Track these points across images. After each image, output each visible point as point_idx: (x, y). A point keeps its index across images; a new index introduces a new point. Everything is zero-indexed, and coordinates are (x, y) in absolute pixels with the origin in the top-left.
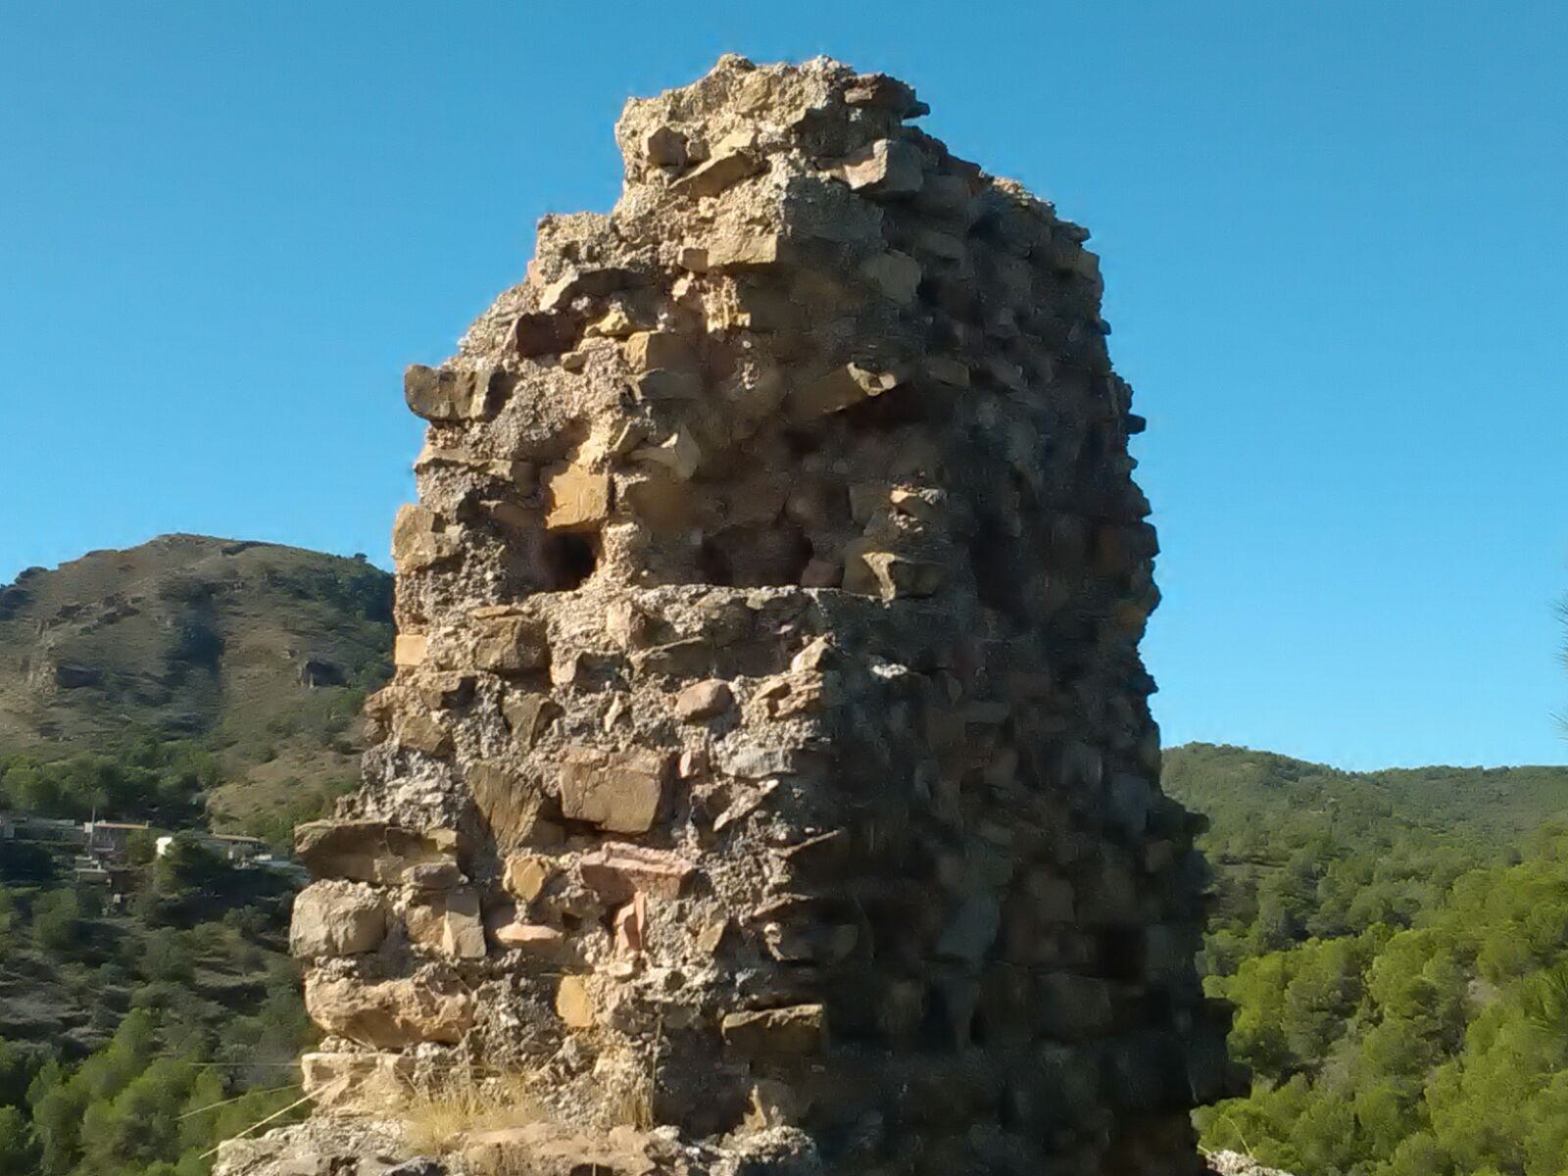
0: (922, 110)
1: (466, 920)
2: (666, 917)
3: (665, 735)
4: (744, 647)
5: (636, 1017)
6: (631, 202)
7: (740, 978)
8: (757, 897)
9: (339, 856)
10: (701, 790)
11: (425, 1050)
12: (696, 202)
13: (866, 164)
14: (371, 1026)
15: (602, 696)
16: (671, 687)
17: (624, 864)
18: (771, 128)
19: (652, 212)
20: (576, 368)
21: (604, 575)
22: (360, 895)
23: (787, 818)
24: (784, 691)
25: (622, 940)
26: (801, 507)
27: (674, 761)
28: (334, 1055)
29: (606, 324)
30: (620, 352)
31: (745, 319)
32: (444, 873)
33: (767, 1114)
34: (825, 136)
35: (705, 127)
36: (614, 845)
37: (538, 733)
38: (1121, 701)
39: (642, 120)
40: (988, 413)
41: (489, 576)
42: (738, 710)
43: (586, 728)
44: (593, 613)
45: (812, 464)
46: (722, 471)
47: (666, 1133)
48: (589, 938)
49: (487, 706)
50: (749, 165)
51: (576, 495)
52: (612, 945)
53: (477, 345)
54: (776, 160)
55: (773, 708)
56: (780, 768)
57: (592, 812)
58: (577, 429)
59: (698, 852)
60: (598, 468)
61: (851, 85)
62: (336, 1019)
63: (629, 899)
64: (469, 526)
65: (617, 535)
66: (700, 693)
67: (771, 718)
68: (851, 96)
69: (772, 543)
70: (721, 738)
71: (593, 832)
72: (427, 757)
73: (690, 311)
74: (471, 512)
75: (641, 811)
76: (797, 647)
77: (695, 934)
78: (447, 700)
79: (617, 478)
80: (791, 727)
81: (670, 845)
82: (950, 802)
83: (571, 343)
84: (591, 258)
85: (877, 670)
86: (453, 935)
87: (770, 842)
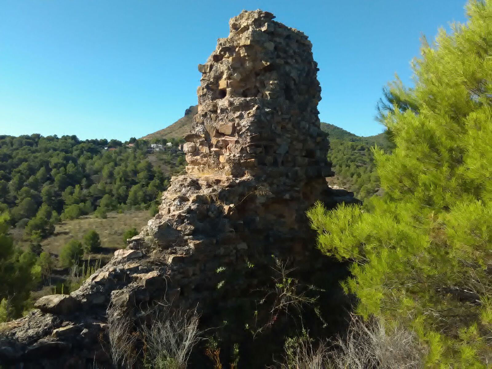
0: (274, 17)
1: (206, 147)
2: (233, 147)
3: (233, 120)
4: (245, 106)
5: (229, 160)
6: (230, 35)
7: (243, 155)
8: (246, 144)
9: (189, 138)
10: (238, 128)
11: (202, 166)
12: (239, 35)
13: (264, 27)
14: (193, 163)
15: (224, 114)
16: (234, 113)
17: (227, 139)
18: (250, 22)
19: (233, 37)
20: (222, 63)
21: (228, 96)
22: (192, 144)
23: (250, 132)
24: (250, 113)
25: (228, 150)
26: (258, 85)
27: (234, 124)
28: (190, 167)
29: (226, 56)
30: (228, 61)
31: (246, 54)
32: (203, 141)
33: (248, 174)
34: (258, 22)
35: (240, 22)
36: (226, 137)
37: (215, 120)
38: (313, 116)
39: (232, 21)
40: (287, 68)
41: (210, 97)
42: (243, 116)
43: (222, 119)
44: (223, 103)
45: (258, 78)
46: (245, 79)
47: (231, 176)
48: (224, 150)
49: (209, 116)
50: (246, 28)
51: (223, 84)
52: (227, 151)
53: (208, 61)
54: (250, 27)
55: (248, 115)
56: (249, 125)
57: (223, 132)
58: (222, 73)
59: (238, 137)
60: (225, 79)
61: (261, 14)
62: (189, 161)
63: (228, 145)
64: (207, 89)
65: (228, 90)
66: (238, 114)
67: (248, 117)
68: (261, 16)
69: (254, 91)
70: (241, 120)
71: (224, 135)
72: (200, 124)
73: (238, 53)
74: (207, 87)
75: (229, 131)
76: (254, 106)
77: (237, 149)
78: (203, 116)
79: (228, 81)
80: (251, 118)
81: (234, 136)
82: (279, 130)
83: (222, 59)
84: (224, 45)
85: (266, 110)
86: (205, 150)
87: (248, 136)
